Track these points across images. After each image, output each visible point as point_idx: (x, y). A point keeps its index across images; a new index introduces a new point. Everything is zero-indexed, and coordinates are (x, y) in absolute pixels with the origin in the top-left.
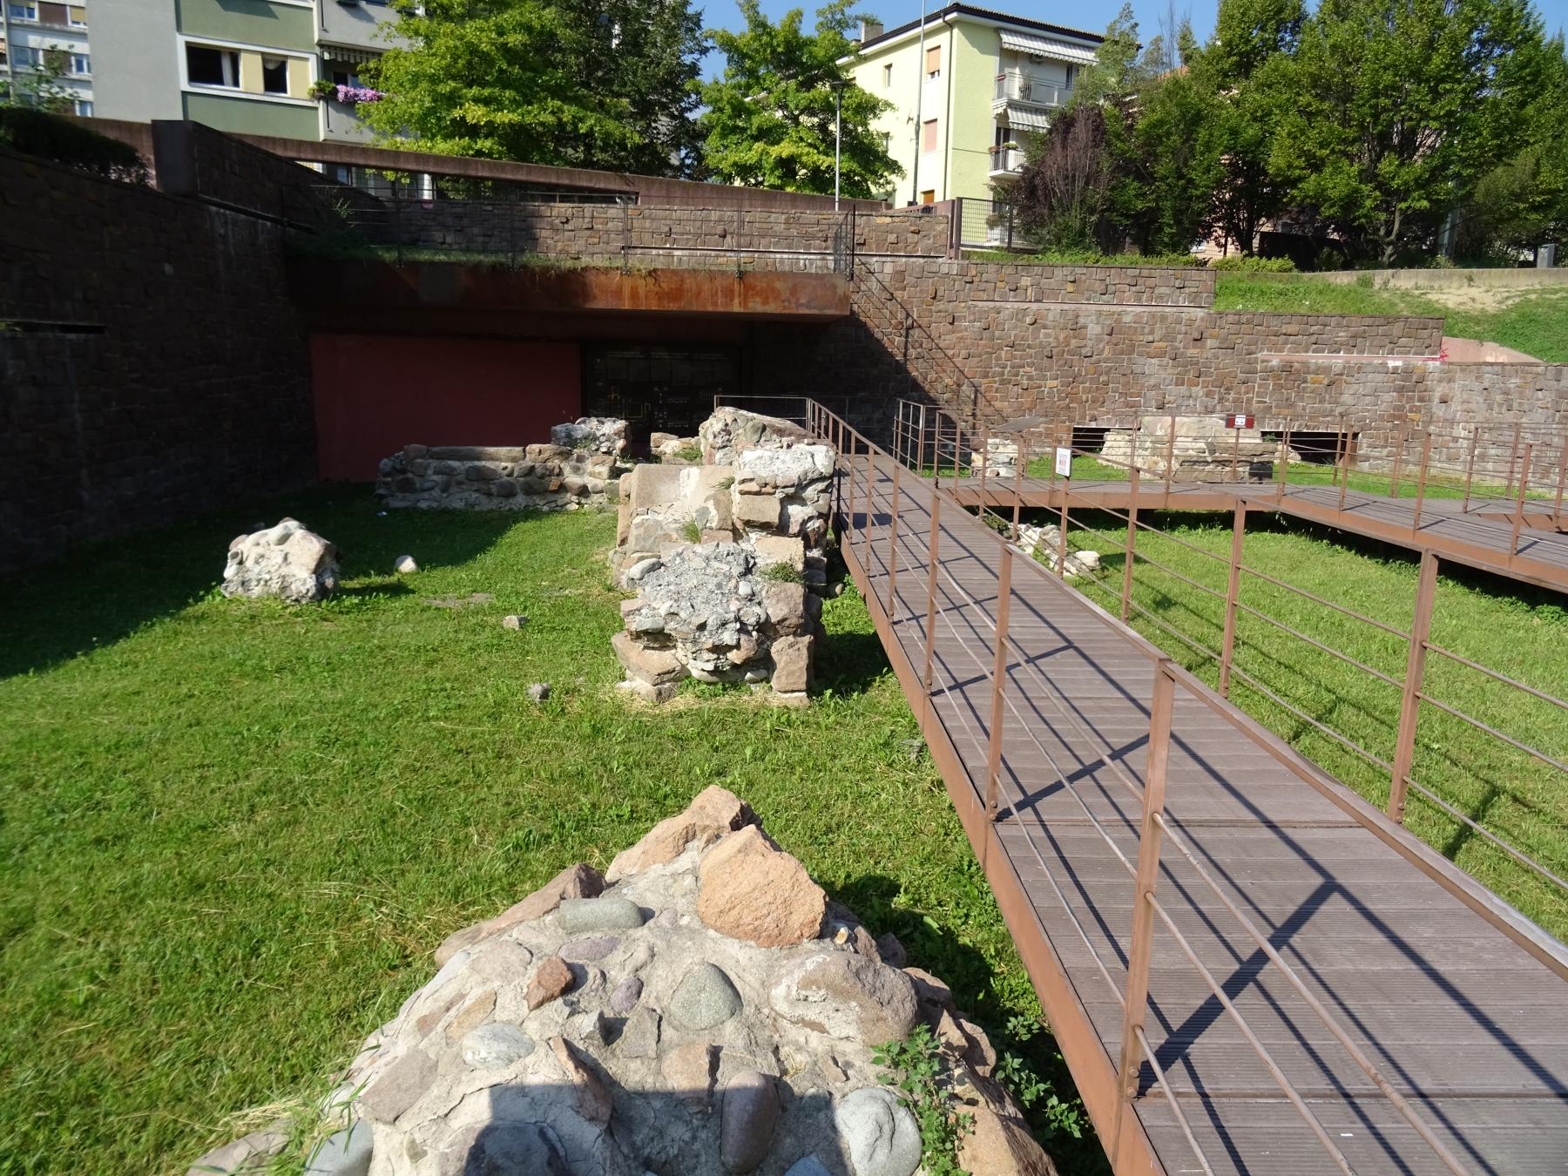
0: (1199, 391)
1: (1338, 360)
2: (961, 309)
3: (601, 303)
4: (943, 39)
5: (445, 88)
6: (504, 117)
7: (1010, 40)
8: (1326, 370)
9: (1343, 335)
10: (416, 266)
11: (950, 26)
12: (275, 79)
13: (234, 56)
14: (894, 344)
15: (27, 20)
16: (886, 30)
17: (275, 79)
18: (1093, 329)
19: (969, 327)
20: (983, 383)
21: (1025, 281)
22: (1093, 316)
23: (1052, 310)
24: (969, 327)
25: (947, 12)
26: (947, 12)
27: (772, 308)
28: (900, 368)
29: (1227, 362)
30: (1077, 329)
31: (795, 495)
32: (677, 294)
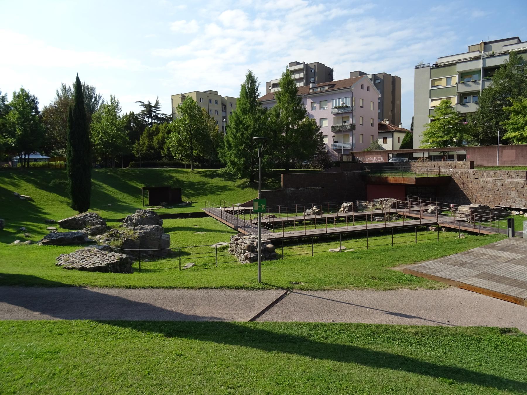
0: (523, 200)
3: (389, 182)
14: (461, 187)
18: (499, 184)
21: (485, 174)
23: (490, 180)
27: (406, 183)
28: (462, 191)
32: (396, 180)
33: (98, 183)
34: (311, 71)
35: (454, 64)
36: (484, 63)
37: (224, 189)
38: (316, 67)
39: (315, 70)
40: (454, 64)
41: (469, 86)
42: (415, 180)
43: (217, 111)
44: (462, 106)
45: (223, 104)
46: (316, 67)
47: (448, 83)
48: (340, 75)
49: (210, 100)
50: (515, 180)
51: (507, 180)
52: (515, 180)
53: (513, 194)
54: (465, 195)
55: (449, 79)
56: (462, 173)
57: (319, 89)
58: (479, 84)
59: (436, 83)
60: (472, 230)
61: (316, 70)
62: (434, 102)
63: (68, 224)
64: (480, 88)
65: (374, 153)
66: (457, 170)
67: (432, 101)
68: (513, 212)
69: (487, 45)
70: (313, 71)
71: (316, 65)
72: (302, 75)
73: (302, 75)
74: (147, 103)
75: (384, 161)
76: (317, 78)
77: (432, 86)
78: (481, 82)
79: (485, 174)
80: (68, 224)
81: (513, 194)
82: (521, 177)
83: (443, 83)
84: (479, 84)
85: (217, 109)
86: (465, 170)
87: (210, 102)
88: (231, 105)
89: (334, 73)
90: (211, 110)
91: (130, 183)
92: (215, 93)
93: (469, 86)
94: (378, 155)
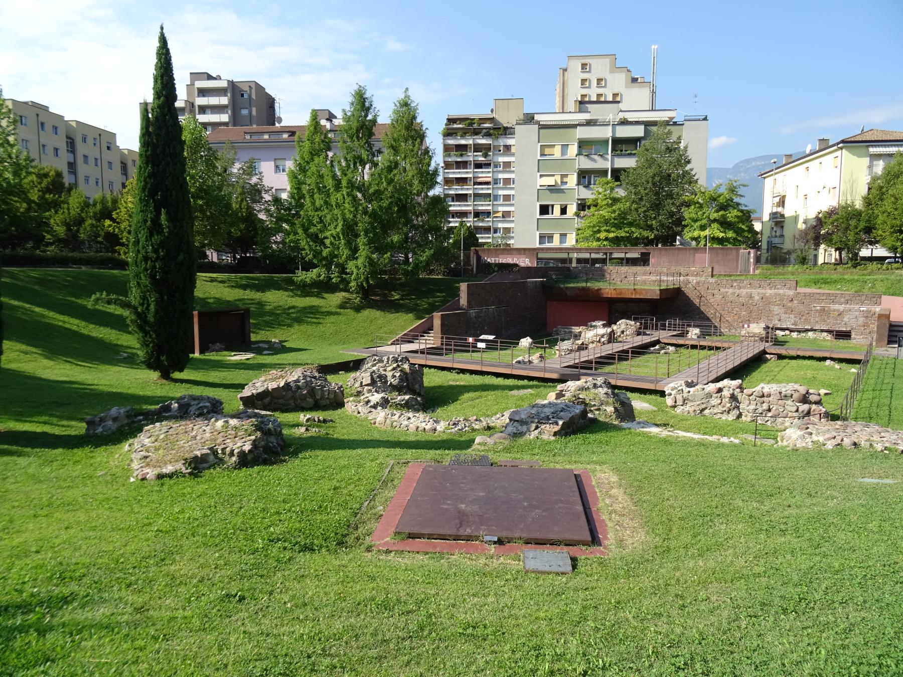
0: (792, 316)
1: (842, 308)
2: (716, 292)
3: (605, 296)
4: (839, 153)
5: (595, 229)
6: (612, 235)
7: (872, 150)
8: (838, 310)
9: (843, 300)
10: (567, 288)
11: (841, 148)
12: (564, 211)
13: (553, 206)
14: (696, 302)
15: (498, 169)
16: (831, 144)
17: (564, 211)
18: (757, 298)
19: (718, 297)
20: (723, 313)
21: (735, 284)
22: (756, 293)
23: (744, 292)
24: (718, 297)
25: (838, 144)
26: (838, 144)
27: (641, 297)
28: (698, 308)
29: (801, 307)
30: (751, 297)
31: (603, 336)
32: (621, 293)
33: (16, 303)
34: (242, 95)
35: (574, 126)
36: (614, 131)
37: (313, 311)
38: (253, 91)
39: (250, 96)
40: (574, 126)
41: (594, 160)
42: (658, 292)
43: (56, 150)
44: (584, 189)
45: (68, 137)
46: (253, 91)
47: (564, 152)
48: (293, 114)
49: (42, 124)
50: (781, 291)
51: (769, 292)
52: (781, 291)
53: (776, 309)
54: (703, 313)
55: (565, 147)
56: (698, 283)
57: (266, 137)
58: (607, 159)
59: (547, 151)
60: (509, 372)
61: (254, 96)
62: (544, 178)
63: (267, 400)
64: (608, 165)
65: (515, 252)
66: (690, 278)
67: (541, 176)
68: (778, 332)
69: (582, 105)
70: (246, 96)
71: (253, 86)
72: (224, 100)
73: (224, 100)
74: (522, 117)
75: (530, 265)
76: (254, 110)
77: (542, 155)
78: (609, 157)
79: (735, 284)
80: (267, 400)
81: (776, 309)
82: (789, 289)
83: (557, 152)
84: (607, 159)
85: (57, 145)
86: (703, 279)
87: (43, 129)
88: (84, 139)
89: (277, 105)
90: (44, 146)
91: (79, 301)
92: (45, 109)
93: (594, 160)
94: (520, 254)
